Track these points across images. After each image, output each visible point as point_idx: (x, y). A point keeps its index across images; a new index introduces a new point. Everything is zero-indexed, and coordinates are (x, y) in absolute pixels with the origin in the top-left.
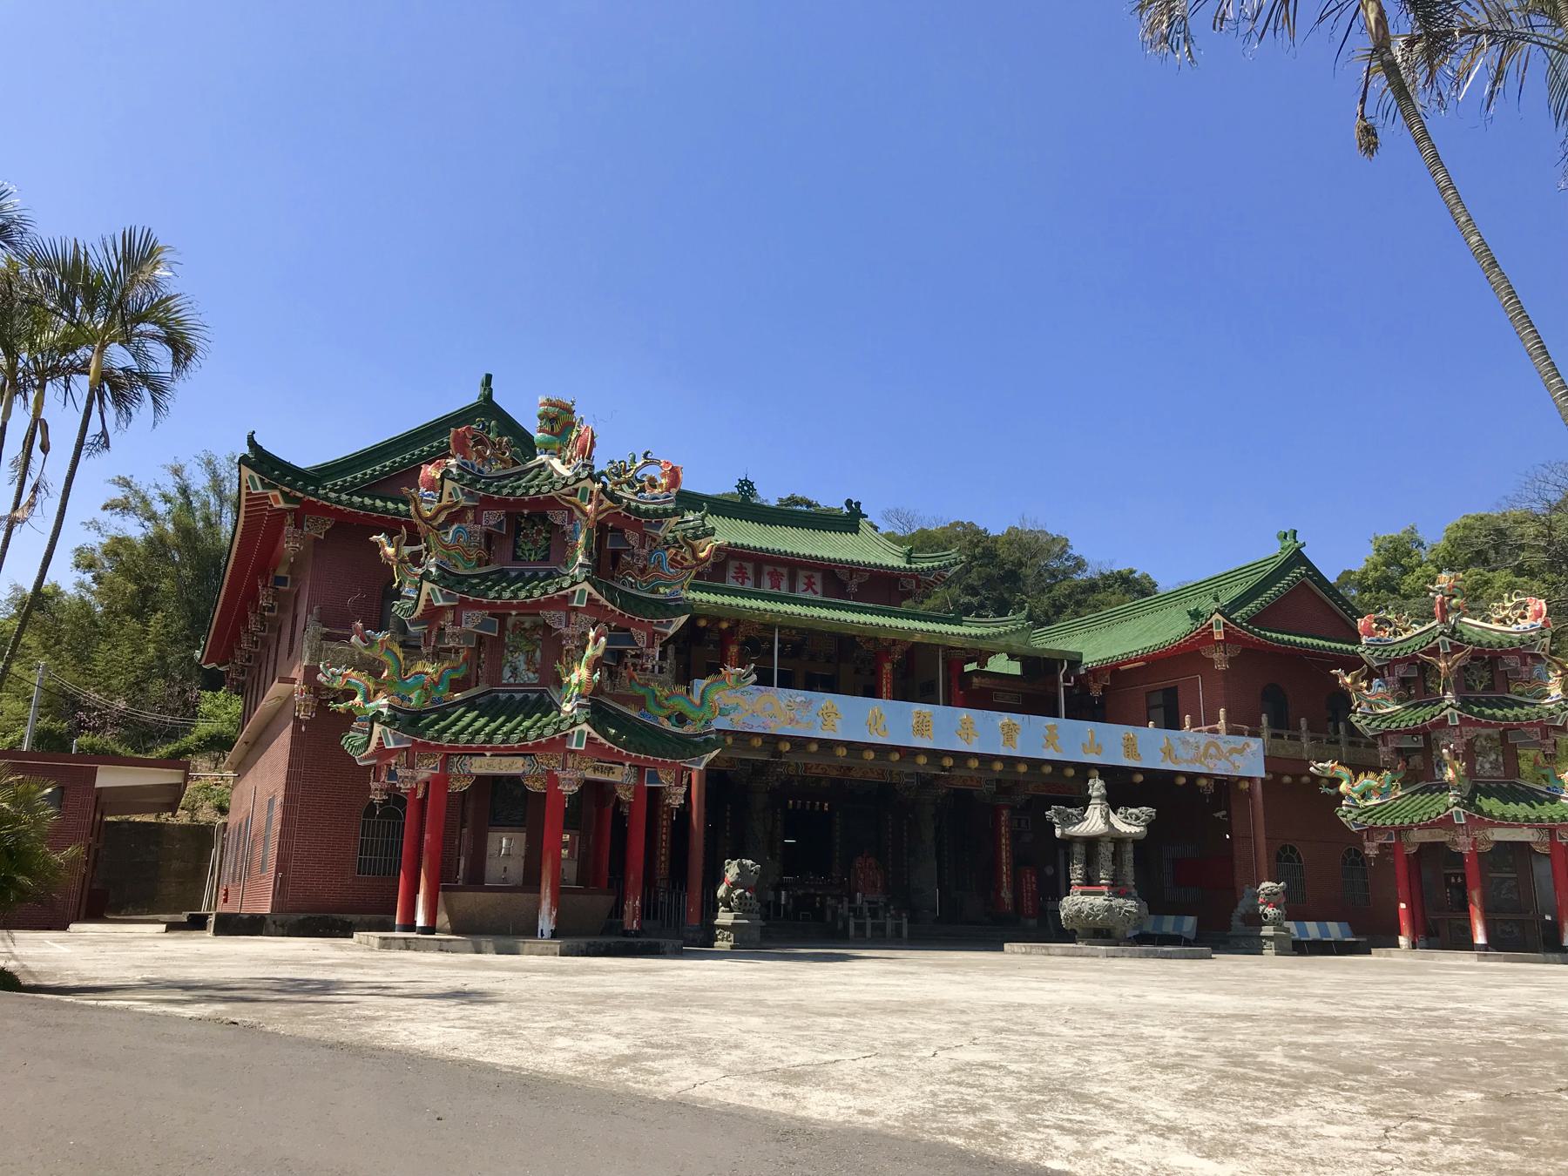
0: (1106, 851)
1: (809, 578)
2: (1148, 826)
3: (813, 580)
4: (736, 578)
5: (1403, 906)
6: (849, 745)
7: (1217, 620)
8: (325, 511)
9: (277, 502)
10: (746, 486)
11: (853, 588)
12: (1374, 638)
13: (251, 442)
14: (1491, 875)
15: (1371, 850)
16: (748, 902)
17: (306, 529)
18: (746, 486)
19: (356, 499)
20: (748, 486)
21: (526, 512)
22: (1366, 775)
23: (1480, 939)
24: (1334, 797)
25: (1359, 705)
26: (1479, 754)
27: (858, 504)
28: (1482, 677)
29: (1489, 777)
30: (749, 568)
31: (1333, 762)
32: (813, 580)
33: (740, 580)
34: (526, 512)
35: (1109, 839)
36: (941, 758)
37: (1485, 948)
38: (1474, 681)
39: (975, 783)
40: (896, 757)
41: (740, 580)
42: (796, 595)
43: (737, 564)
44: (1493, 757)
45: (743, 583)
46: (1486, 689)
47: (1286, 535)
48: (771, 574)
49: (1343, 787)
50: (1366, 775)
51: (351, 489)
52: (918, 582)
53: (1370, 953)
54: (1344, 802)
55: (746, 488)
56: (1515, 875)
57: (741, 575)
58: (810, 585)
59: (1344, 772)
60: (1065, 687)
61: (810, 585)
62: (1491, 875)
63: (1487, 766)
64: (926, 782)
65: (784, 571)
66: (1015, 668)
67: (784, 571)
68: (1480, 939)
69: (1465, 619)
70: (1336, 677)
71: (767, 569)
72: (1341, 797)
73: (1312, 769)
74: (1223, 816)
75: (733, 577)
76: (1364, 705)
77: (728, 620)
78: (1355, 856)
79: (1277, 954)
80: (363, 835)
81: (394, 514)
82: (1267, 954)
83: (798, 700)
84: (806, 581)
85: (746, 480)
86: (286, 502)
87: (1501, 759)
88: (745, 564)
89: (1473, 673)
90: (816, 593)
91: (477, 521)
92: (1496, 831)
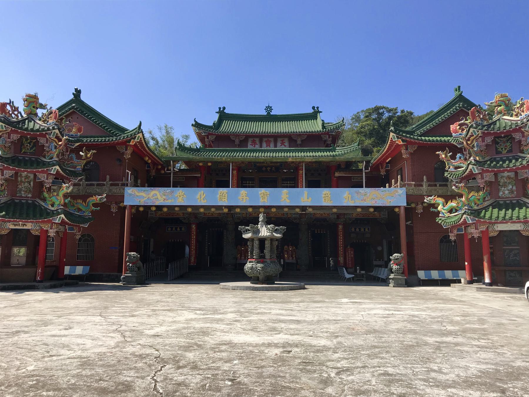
0: (267, 244)
1: (282, 141)
2: (284, 234)
3: (284, 141)
4: (252, 145)
5: (466, 263)
6: (168, 207)
7: (393, 135)
8: (415, 143)
9: (400, 142)
10: (269, 109)
11: (299, 142)
12: (458, 134)
13: (195, 121)
14: (505, 247)
15: (452, 238)
16: (133, 268)
17: (409, 150)
18: (269, 109)
19: (423, 138)
20: (269, 108)
21: (503, 135)
22: (451, 202)
23: (487, 280)
24: (437, 212)
25: (449, 168)
26: (502, 186)
27: (318, 108)
28: (506, 146)
29: (511, 198)
30: (257, 140)
31: (435, 197)
32: (284, 141)
33: (253, 145)
34: (503, 135)
35: (257, 239)
36: (247, 209)
37: (490, 284)
38: (502, 149)
39: (326, 215)
40: (213, 210)
41: (253, 145)
42: (278, 148)
43: (252, 139)
44: (511, 187)
45: (255, 146)
46: (508, 152)
47: (456, 89)
48: (266, 142)
49: (439, 208)
50: (451, 202)
51: (424, 134)
52: (329, 135)
53: (450, 286)
54: (440, 215)
55: (269, 109)
56: (518, 247)
57: (254, 143)
58: (283, 144)
59: (440, 201)
60: (365, 172)
61: (283, 144)
62: (505, 247)
63: (507, 192)
64: (338, 216)
65: (272, 139)
66: (183, 167)
67: (272, 139)
68: (487, 280)
69: (505, 117)
70: (439, 155)
71: (265, 139)
72: (439, 212)
73: (425, 200)
74: (410, 224)
75: (251, 145)
76: (451, 167)
77: (210, 162)
78: (445, 239)
79: (394, 286)
80: (78, 248)
81: (444, 142)
82: (391, 286)
83: (168, 191)
84: (281, 142)
85: (269, 106)
86: (403, 142)
87: (514, 188)
88: (255, 139)
89: (501, 145)
90: (285, 146)
91: (483, 141)
92: (499, 225)
